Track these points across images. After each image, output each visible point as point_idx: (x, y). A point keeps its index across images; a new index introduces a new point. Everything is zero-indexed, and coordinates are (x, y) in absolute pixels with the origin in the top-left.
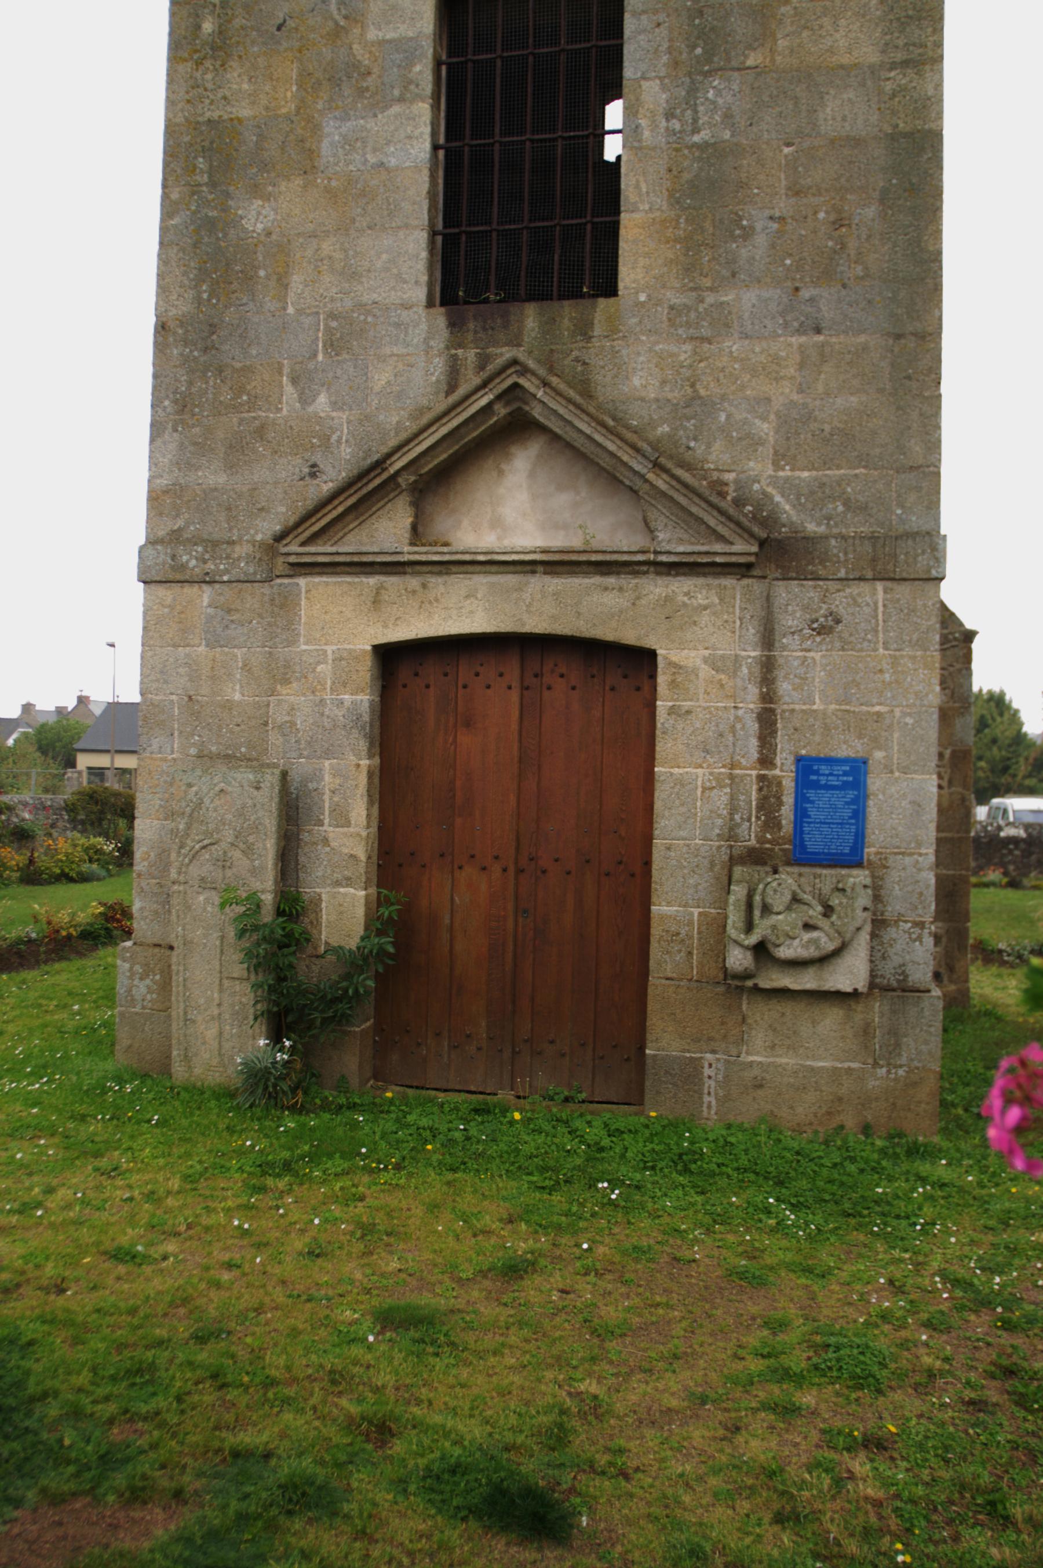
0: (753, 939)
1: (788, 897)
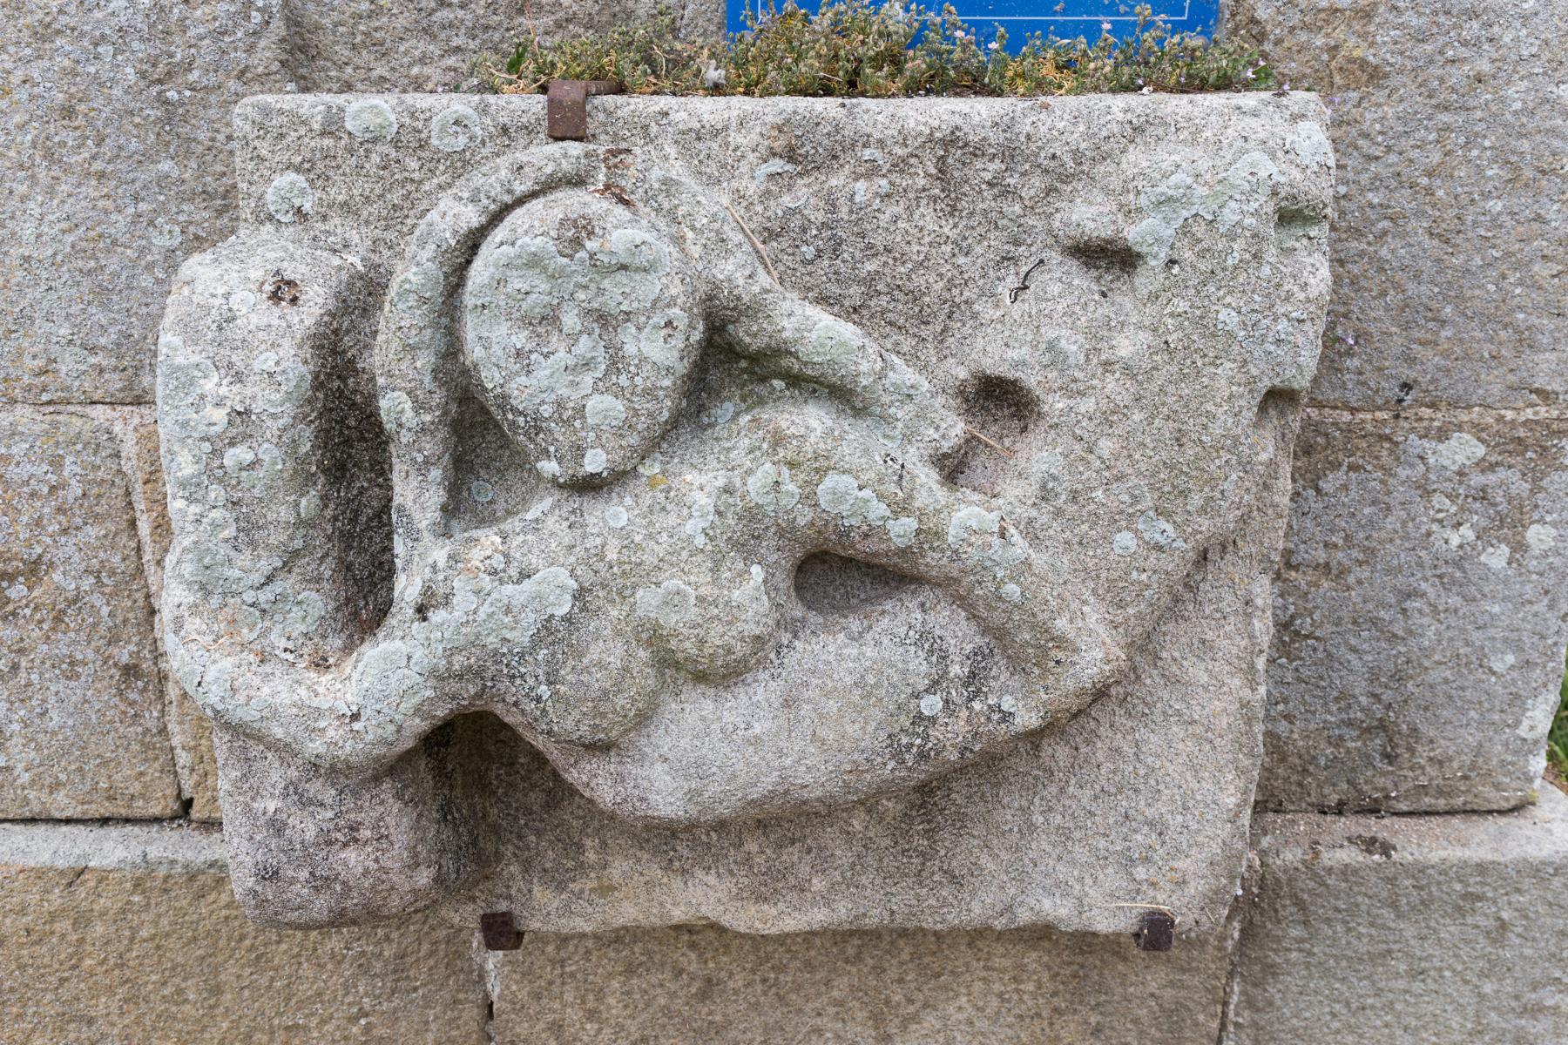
0: (382, 686)
1: (660, 351)
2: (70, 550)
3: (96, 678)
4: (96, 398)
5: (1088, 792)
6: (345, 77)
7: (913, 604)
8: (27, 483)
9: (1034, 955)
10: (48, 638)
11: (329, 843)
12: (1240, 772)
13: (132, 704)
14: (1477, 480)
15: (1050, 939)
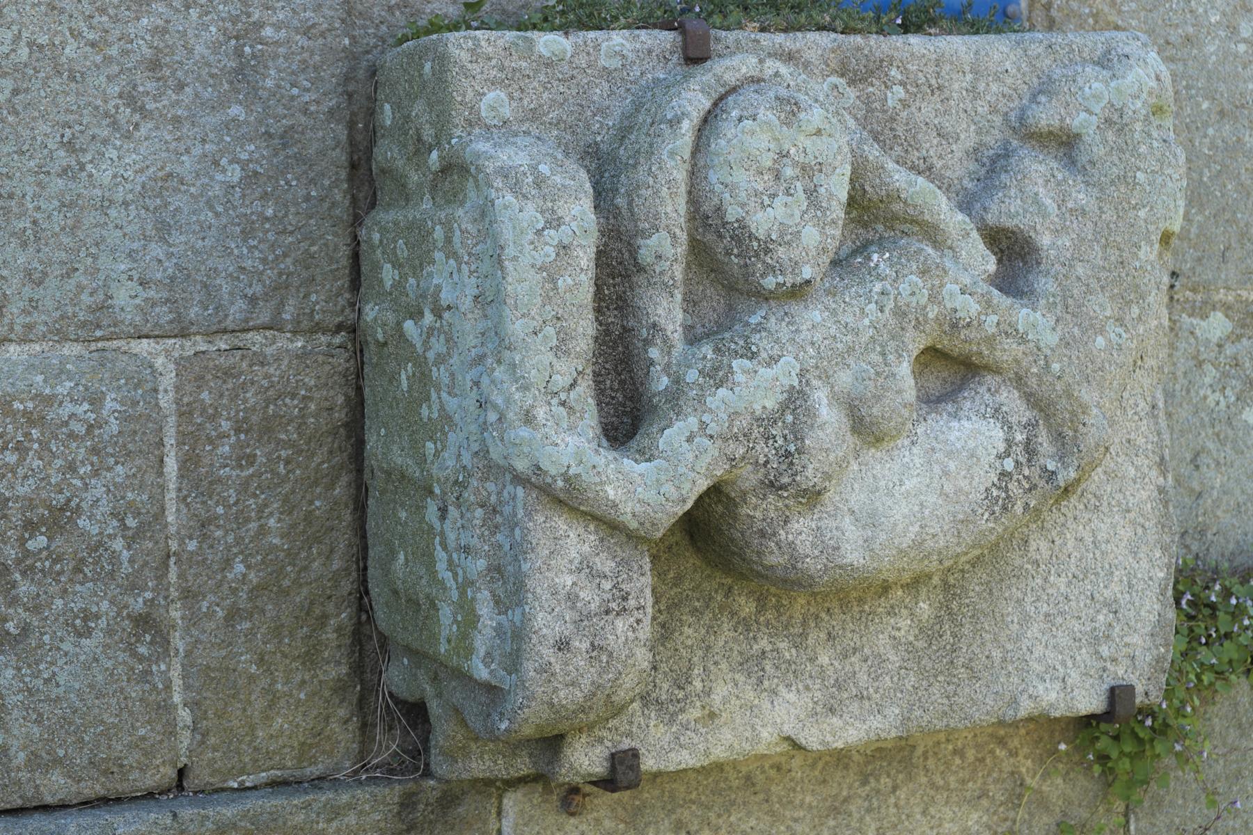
2: (100, 491)
3: (110, 632)
4: (145, 331)
5: (1063, 579)
6: (380, 34)
7: (982, 390)
8: (66, 424)
9: (975, 816)
10: (65, 591)
11: (607, 612)
12: (1165, 549)
13: (141, 659)
14: (1229, 350)
15: (988, 796)
